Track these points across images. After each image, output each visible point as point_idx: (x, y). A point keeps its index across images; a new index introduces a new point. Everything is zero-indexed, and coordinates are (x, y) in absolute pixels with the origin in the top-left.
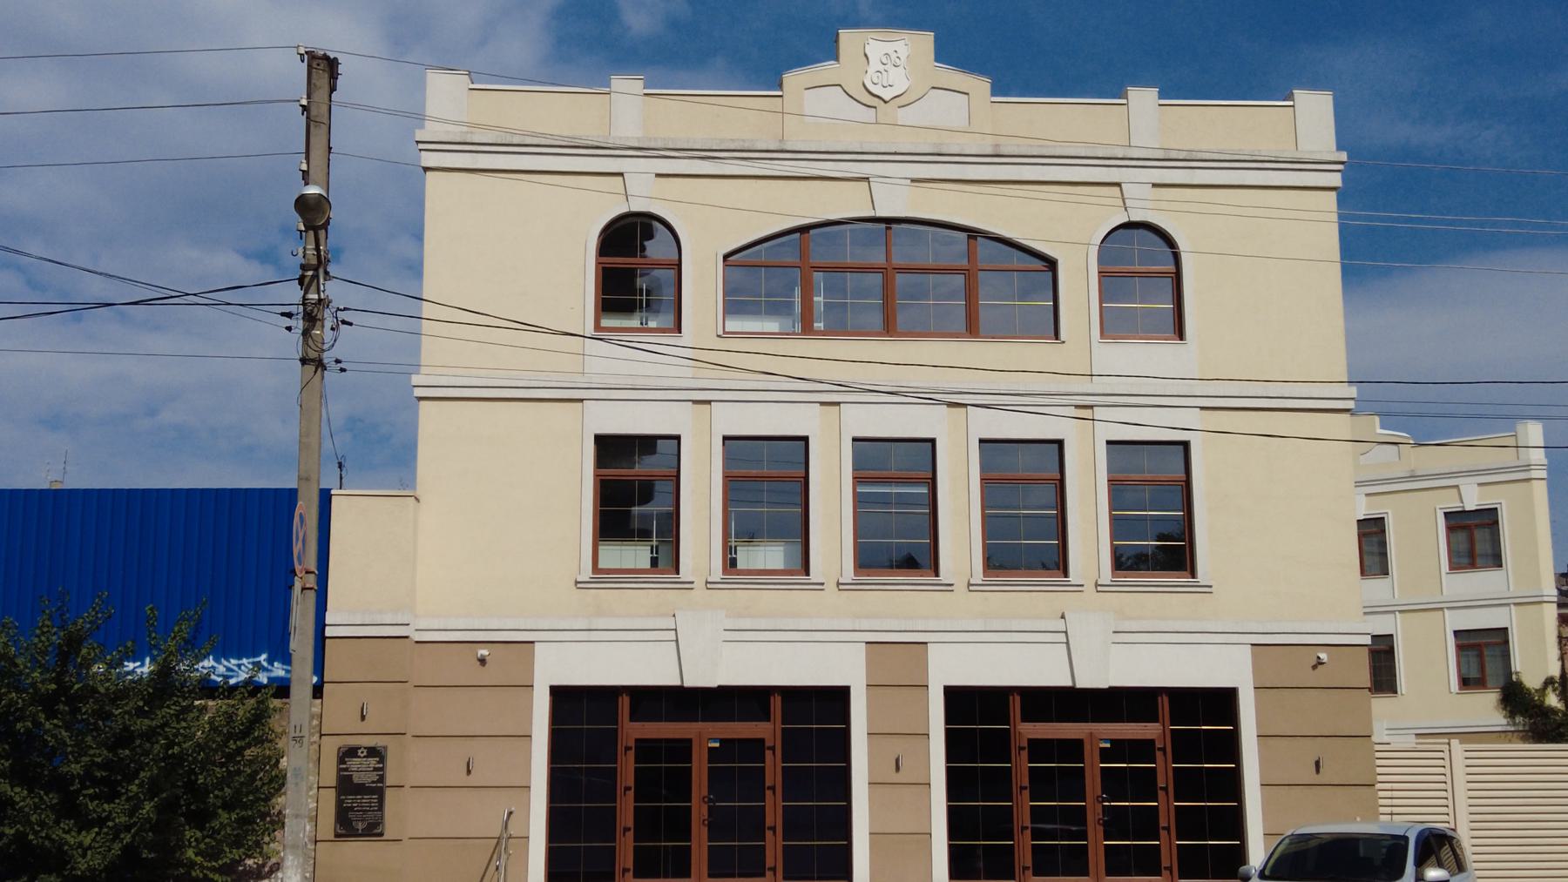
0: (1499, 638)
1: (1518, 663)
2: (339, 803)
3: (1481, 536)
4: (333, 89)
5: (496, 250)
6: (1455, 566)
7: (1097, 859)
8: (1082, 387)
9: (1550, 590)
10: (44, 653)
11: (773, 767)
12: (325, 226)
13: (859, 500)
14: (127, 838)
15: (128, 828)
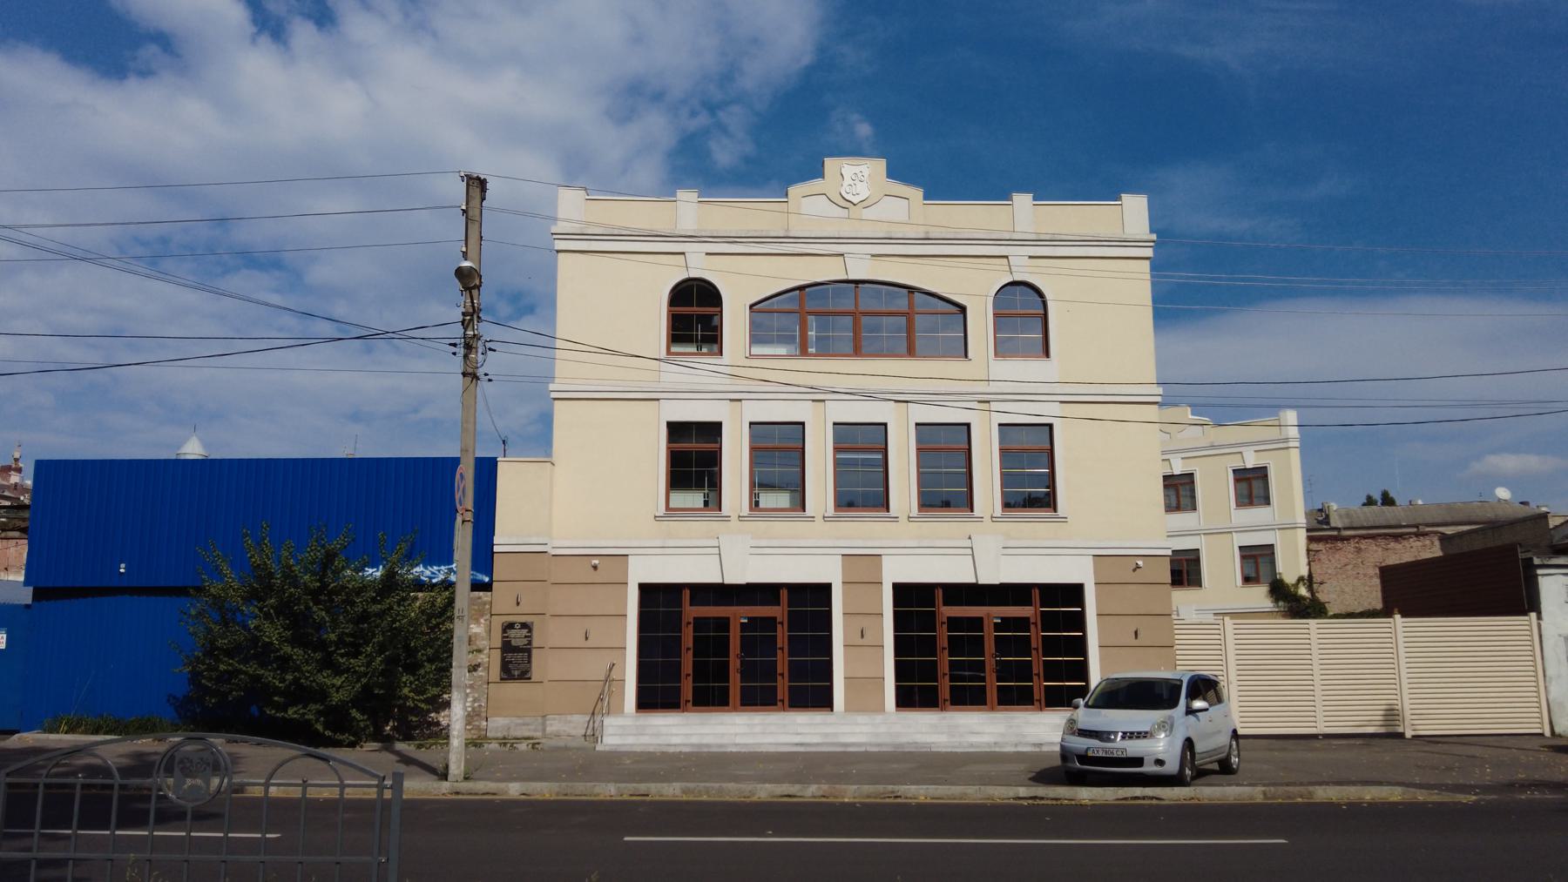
0: (1269, 550)
1: (1281, 567)
2: (503, 659)
3: (1257, 485)
4: (483, 199)
5: (607, 305)
6: (1239, 504)
7: (992, 694)
8: (981, 388)
9: (1301, 519)
10: (312, 563)
11: (782, 635)
12: (478, 287)
13: (837, 463)
14: (364, 680)
15: (365, 675)
